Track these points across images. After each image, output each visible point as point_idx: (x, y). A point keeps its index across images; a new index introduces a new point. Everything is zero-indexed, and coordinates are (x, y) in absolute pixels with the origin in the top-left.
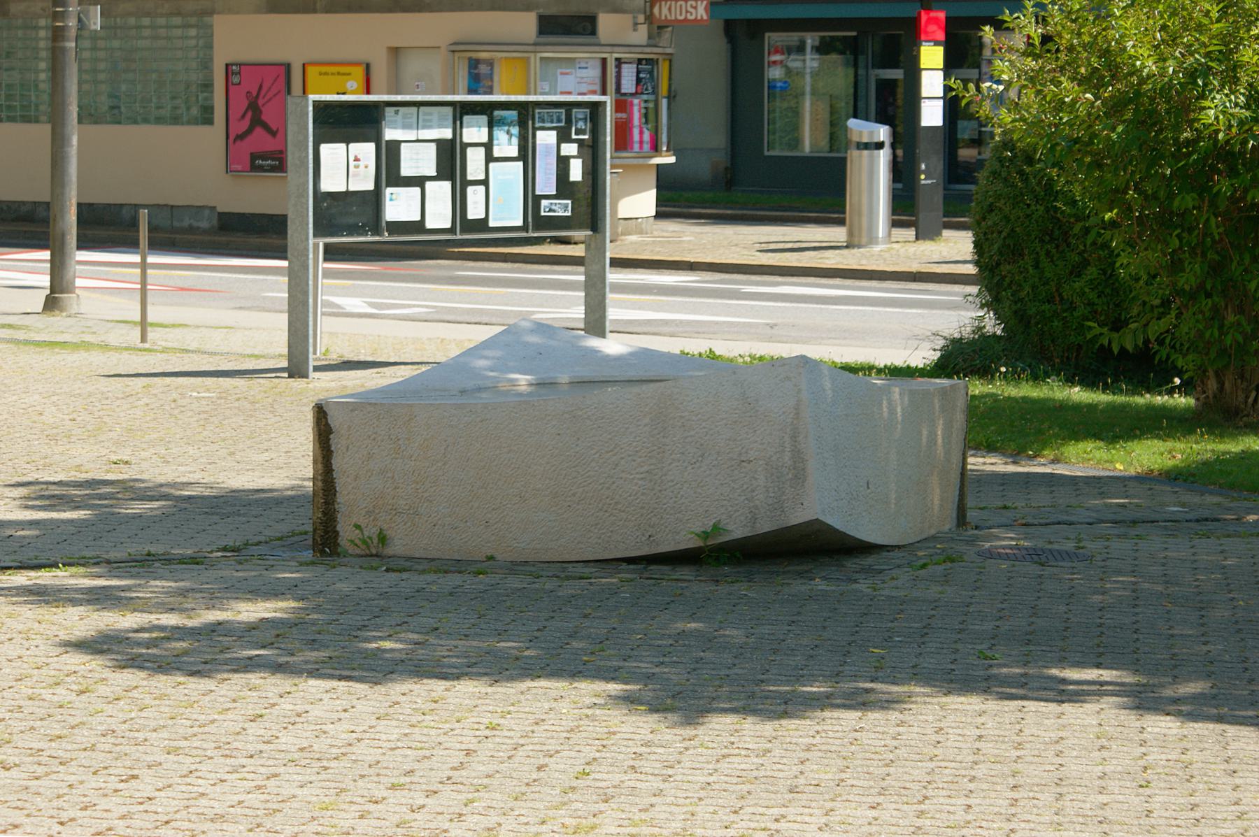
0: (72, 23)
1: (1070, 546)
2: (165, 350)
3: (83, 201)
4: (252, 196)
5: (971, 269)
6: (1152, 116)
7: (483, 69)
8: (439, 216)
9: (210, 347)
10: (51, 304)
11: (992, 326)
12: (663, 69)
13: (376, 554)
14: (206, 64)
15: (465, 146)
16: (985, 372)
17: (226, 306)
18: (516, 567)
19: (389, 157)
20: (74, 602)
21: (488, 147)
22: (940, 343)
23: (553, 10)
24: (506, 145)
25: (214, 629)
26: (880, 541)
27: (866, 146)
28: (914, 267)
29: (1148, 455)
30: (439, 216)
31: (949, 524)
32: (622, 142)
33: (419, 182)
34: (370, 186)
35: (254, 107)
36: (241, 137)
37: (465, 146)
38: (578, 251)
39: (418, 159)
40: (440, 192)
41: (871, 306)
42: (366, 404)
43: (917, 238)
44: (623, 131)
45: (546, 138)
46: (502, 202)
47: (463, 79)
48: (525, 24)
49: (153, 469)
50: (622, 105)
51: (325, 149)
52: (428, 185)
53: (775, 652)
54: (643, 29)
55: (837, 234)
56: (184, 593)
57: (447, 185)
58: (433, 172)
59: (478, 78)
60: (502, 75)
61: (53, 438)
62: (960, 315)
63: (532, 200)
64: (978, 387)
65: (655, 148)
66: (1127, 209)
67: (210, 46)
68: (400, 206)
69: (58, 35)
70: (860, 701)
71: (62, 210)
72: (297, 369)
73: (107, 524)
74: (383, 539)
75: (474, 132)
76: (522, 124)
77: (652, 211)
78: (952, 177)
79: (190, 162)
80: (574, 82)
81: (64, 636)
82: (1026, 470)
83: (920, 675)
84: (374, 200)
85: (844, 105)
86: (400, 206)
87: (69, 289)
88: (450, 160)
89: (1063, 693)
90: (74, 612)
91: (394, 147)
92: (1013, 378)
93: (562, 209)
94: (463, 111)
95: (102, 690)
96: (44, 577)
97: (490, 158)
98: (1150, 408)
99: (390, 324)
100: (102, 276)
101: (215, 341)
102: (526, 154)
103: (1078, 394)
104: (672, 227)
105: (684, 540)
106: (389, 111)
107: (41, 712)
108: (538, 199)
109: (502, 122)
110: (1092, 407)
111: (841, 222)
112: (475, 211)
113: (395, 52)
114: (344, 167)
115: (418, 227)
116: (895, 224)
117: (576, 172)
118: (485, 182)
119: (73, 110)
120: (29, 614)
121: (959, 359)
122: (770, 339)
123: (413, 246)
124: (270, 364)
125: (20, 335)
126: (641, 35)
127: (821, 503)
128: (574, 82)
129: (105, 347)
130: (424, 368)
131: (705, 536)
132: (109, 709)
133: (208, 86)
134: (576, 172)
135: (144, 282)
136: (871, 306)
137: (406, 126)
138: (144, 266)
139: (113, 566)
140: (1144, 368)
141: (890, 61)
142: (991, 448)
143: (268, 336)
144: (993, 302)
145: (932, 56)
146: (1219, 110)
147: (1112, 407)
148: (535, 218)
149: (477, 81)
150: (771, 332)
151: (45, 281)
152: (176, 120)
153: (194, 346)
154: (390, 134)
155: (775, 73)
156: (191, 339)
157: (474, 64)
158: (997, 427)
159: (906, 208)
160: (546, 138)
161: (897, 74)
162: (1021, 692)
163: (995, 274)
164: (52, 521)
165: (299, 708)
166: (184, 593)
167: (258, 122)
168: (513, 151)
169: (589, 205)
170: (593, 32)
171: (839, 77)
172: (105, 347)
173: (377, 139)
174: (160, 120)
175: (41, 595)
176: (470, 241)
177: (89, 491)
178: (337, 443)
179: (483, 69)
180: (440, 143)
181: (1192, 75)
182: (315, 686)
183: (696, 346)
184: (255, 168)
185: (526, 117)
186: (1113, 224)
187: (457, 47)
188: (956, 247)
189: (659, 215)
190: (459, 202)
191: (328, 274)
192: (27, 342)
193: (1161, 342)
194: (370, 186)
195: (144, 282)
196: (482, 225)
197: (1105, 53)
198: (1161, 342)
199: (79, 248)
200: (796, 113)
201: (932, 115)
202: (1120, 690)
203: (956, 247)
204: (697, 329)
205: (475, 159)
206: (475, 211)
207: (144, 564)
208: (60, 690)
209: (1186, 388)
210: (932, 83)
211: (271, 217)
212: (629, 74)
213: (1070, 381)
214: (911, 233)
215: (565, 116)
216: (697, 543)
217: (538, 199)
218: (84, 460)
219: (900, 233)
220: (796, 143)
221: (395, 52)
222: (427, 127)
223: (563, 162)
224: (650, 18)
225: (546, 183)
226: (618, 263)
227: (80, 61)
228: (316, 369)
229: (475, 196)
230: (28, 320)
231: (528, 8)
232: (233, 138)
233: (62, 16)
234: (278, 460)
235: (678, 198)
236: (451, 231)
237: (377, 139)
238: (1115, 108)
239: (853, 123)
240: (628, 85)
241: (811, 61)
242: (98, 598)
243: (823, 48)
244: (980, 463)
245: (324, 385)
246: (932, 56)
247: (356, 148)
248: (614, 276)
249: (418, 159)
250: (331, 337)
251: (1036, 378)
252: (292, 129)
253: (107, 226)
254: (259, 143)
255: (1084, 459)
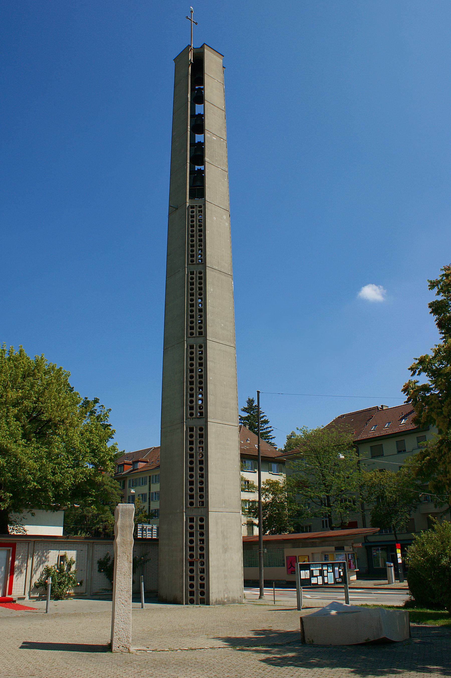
0: (262, 551)
1: (429, 641)
2: (278, 606)
3: (265, 579)
4: (290, 578)
5: (408, 587)
6: (433, 562)
7: (327, 556)
8: (320, 582)
9: (285, 605)
10: (260, 598)
11: (413, 598)
12: (355, 555)
13: (312, 644)
14: (283, 557)
15: (324, 570)
16: (413, 607)
17: (286, 598)
18: (335, 646)
19: (311, 572)
20: (262, 653)
21: (327, 570)
22: (404, 602)
23: (337, 546)
24: (330, 570)
25: (286, 657)
26: (396, 641)
27: (389, 567)
28: (400, 587)
29: (441, 622)
30: (320, 582)
31: (408, 637)
32: (350, 567)
33: (317, 576)
34: (309, 577)
35: (291, 563)
36: (289, 568)
37: (324, 570)
38: (343, 586)
39: (316, 573)
40: (320, 578)
41: (392, 595)
42: (307, 617)
43: (400, 582)
44: (350, 565)
45: (336, 568)
46: (330, 579)
47: (324, 558)
48: (333, 548)
49: (275, 628)
50: (349, 561)
51: (301, 572)
52: (318, 577)
53: (379, 663)
54: (352, 549)
55: (386, 581)
56: (280, 651)
57: (321, 577)
58: (319, 575)
59: (326, 559)
60: (330, 557)
61: (260, 622)
62: (406, 597)
63: (335, 579)
64: (411, 610)
65: (355, 568)
66: (432, 578)
67: (284, 554)
68: (314, 581)
69: (260, 553)
70: (394, 672)
71: (262, 582)
72: (299, 609)
73: (268, 638)
74: (313, 641)
75: (325, 568)
76: (332, 566)
77: (356, 579)
78: (403, 572)
79: (281, 572)
80: (341, 559)
81: (260, 659)
82: (421, 626)
83: (404, 668)
84: (310, 579)
85: (386, 559)
86: (314, 581)
87: (263, 595)
88: (321, 573)
89: (430, 671)
90: (263, 655)
91: (312, 570)
92: (417, 608)
93: (340, 580)
94: (323, 565)
95: (267, 670)
96: (258, 648)
97: (328, 572)
98: (441, 613)
99: (315, 601)
100: (268, 592)
101: (286, 604)
102: (334, 571)
103: (429, 611)
104: (359, 581)
105: (363, 641)
106: (311, 565)
107: (257, 674)
108: (336, 579)
109: (329, 566)
110: (431, 613)
111: (387, 579)
112: (326, 581)
113: (313, 554)
114: (304, 574)
115: (317, 584)
116: (396, 579)
117: (342, 574)
118: (327, 576)
119: (263, 565)
120: (255, 655)
121: (408, 605)
122: (377, 601)
123: (316, 586)
124: (295, 608)
125: (255, 603)
126: (351, 550)
127: (385, 634)
128: (341, 559)
129: (268, 605)
130: (320, 609)
131: (366, 640)
132: (268, 674)
133: (284, 560)
134: (342, 574)
135: (274, 593)
136: (392, 595)
137: (314, 567)
138: (274, 590)
139: (269, 646)
140: (439, 606)
141: (393, 552)
142: (413, 622)
143: (293, 602)
144: (413, 595)
145: (399, 551)
146: (444, 561)
147: (435, 613)
148: (336, 582)
149: (326, 559)
150: (377, 600)
151: (259, 593)
152: (279, 566)
153: (282, 605)
154: (311, 569)
155: (375, 554)
156: (282, 603)
157: (325, 555)
158: (414, 617)
159: (397, 577)
160: (336, 568)
161: (394, 554)
162: (420, 670)
163: (412, 588)
164: (259, 637)
165: (299, 674)
166: (280, 651)
167: (292, 566)
168: (331, 571)
169: (344, 579)
170: (344, 549)
171: (385, 554)
172: (268, 605)
173: (310, 570)
174: (276, 566)
175: (257, 651)
176: (325, 585)
177: (264, 632)
178: (304, 624)
179: (327, 556)
180: (319, 570)
181: (439, 555)
182: (302, 669)
183: (364, 603)
184: (292, 573)
185: (333, 565)
186: (430, 581)
187: (322, 552)
188: (405, 584)
189: (357, 579)
190: (323, 580)
191: (303, 591)
192: (256, 604)
193: (441, 602)
194: (309, 577)
195: (274, 593)
196: (327, 583)
197: (425, 551)
198: (441, 602)
199: (264, 587)
200: (378, 560)
201: (400, 561)
202: (441, 670)
203: (405, 584)
204: (365, 600)
205: (325, 572)
206: (326, 581)
207: (274, 646)
208: (260, 670)
209: (447, 610)
210: (399, 555)
211: (293, 581)
212: (350, 556)
213: (427, 608)
214: (399, 581)
215: (339, 565)
216: (365, 642)
217: (336, 579)
218: (265, 626)
219: (396, 581)
220: (379, 565)
221: (313, 554)
222: (317, 567)
223: (340, 572)
224: (352, 546)
225: (337, 576)
226: (350, 588)
227: (264, 558)
228: (302, 609)
229: (326, 578)
230: (257, 600)
231: (333, 546)
232: (288, 568)
233: (261, 550)
234: (294, 626)
235: (359, 577)
236: (322, 585)
237: (310, 570)
238: (428, 560)
239: (387, 563)
240: (350, 558)
241: (380, 552)
242: (266, 652)
243: (382, 550)
244: (412, 624)
245: (304, 613)
246: (399, 551)
247: (306, 571)
248: (349, 590)
249: (316, 573)
250: (305, 602)
251: (422, 608)
252: (296, 568)
253: (268, 584)
254: (292, 570)
255: (430, 624)
